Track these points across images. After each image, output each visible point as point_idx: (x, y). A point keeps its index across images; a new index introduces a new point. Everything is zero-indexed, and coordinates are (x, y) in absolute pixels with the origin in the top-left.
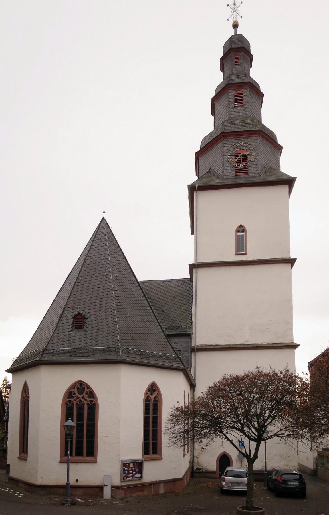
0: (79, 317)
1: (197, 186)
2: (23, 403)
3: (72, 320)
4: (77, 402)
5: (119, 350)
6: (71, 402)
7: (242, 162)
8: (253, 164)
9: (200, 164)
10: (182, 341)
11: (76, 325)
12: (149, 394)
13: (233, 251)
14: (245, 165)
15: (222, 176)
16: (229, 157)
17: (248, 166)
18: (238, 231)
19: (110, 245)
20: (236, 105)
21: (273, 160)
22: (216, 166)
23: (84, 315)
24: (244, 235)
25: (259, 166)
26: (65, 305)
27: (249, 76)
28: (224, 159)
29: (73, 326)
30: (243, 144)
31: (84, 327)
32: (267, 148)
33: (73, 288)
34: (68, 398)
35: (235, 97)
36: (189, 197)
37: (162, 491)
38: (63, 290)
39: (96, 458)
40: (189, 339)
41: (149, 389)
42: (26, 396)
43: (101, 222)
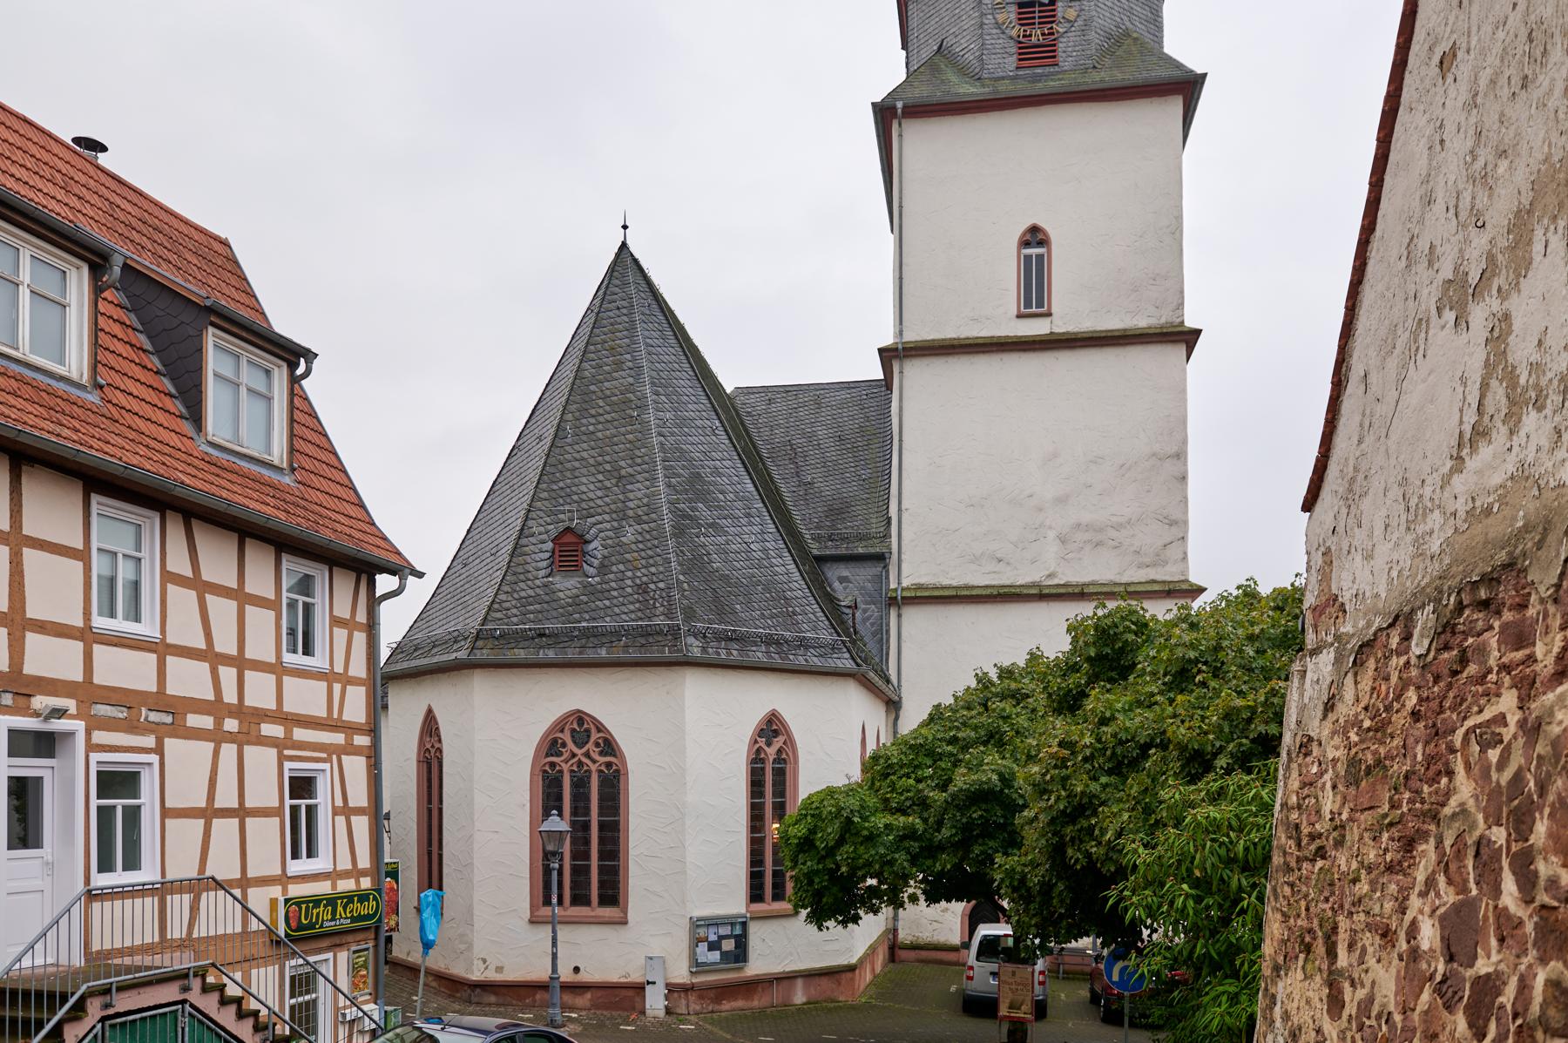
0: (569, 538)
1: (899, 105)
2: (425, 765)
3: (550, 545)
4: (572, 765)
5: (680, 629)
6: (555, 766)
7: (1039, 23)
8: (1073, 29)
9: (913, 23)
11: (560, 561)
12: (762, 742)
13: (1011, 303)
14: (1049, 34)
15: (977, 70)
17: (1056, 36)
18: (1025, 243)
19: (645, 326)
22: (960, 37)
23: (580, 533)
25: (1092, 35)
26: (528, 502)
28: (983, 15)
31: (582, 566)
33: (548, 456)
36: (878, 136)
37: (799, 997)
39: (625, 912)
41: (762, 730)
42: (433, 746)
43: (618, 255)
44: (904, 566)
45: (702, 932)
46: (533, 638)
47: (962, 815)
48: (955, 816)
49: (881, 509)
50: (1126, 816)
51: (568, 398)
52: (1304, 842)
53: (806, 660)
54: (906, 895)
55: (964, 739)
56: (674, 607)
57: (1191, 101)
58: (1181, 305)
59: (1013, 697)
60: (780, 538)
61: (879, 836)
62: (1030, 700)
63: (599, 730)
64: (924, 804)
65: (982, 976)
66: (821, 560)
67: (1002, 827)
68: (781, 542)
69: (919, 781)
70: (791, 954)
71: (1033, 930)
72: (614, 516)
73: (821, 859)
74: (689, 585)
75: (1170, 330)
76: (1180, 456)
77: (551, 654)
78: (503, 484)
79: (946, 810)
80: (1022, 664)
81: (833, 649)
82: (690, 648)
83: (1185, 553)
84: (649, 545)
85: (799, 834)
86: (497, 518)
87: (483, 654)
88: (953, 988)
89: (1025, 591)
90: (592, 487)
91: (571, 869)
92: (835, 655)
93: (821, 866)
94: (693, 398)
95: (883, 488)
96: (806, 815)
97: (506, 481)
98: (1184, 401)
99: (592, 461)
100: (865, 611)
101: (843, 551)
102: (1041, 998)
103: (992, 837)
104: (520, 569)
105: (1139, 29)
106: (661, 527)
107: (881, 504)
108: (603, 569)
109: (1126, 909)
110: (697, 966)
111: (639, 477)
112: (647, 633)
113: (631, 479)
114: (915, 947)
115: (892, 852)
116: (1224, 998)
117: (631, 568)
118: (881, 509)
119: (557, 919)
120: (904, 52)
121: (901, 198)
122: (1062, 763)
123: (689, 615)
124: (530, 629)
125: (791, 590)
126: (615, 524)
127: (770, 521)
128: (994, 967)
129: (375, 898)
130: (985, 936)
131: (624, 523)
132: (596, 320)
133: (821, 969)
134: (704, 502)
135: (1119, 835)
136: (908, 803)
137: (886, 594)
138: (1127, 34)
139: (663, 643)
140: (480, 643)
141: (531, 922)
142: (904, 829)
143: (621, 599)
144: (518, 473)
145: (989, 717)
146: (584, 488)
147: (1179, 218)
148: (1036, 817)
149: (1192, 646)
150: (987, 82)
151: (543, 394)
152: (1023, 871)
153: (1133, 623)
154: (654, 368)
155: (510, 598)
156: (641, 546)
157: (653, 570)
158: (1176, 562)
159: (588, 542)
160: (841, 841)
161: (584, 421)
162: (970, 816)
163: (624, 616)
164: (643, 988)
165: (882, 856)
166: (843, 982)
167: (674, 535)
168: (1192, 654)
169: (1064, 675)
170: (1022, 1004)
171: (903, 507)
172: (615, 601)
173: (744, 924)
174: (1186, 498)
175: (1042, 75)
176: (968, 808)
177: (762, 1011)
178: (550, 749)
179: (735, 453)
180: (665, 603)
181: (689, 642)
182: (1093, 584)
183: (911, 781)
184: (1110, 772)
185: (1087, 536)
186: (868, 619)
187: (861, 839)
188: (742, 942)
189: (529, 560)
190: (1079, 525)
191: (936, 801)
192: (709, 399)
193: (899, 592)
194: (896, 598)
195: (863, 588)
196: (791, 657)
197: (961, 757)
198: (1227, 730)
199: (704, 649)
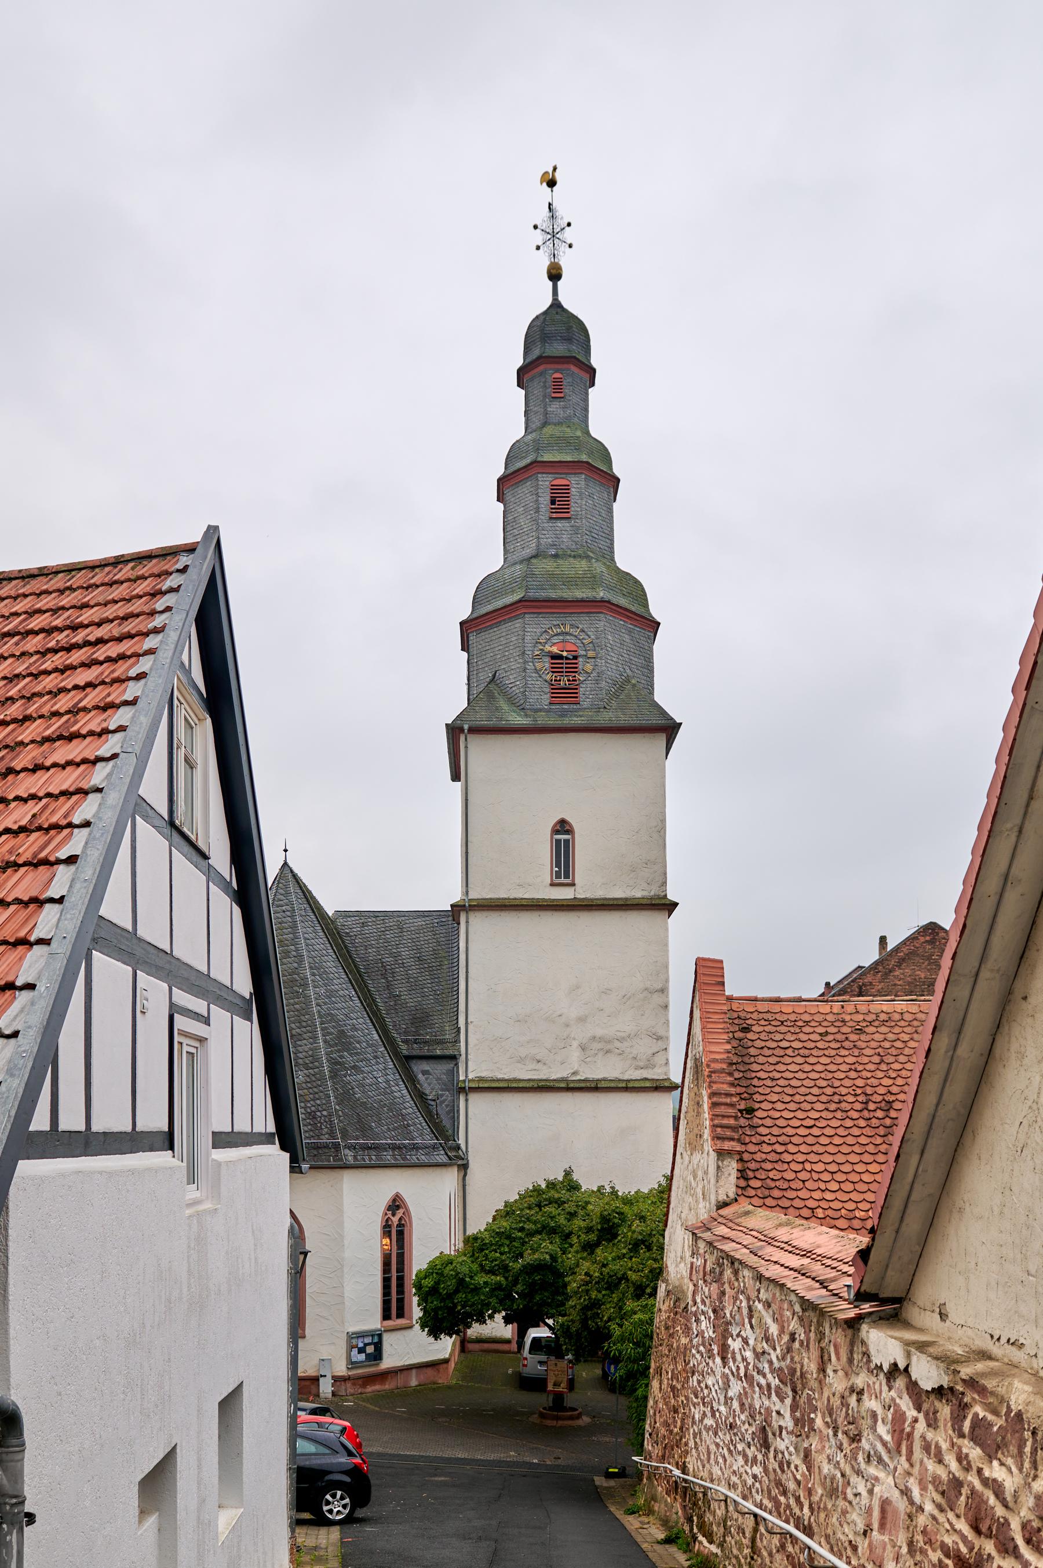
1: (466, 727)
10: (440, 1069)
15: (522, 702)
18: (555, 831)
20: (554, 515)
21: (636, 660)
28: (525, 662)
30: (567, 630)
37: (414, 1382)
44: (470, 1063)
45: (354, 1342)
47: (529, 1278)
49: (452, 1019)
50: (612, 1310)
53: (417, 1158)
55: (529, 1230)
58: (664, 883)
59: (556, 1202)
64: (506, 1268)
65: (532, 1364)
66: (409, 1058)
70: (408, 1353)
73: (443, 1300)
75: (657, 902)
76: (663, 990)
80: (561, 1179)
81: (433, 1148)
83: (667, 1060)
84: (315, 1084)
88: (510, 1371)
89: (557, 1085)
96: (432, 1273)
106: (322, 1072)
107: (452, 1014)
110: (352, 1364)
111: (305, 1036)
113: (299, 1037)
114: (480, 1341)
118: (452, 1019)
120: (465, 655)
122: (587, 1283)
125: (405, 1108)
128: (543, 1358)
130: (534, 1338)
133: (427, 1362)
134: (347, 1050)
135: (609, 1320)
136: (496, 1268)
145: (543, 1216)
147: (663, 821)
150: (529, 713)
153: (617, 1213)
156: (309, 1085)
157: (318, 1102)
160: (457, 1291)
164: (318, 1380)
165: (482, 1300)
166: (441, 1370)
167: (331, 1077)
168: (640, 1237)
169: (587, 1232)
171: (469, 1021)
173: (380, 1336)
174: (668, 1021)
177: (392, 1391)
182: (605, 1080)
184: (606, 1289)
185: (599, 1046)
188: (378, 1346)
192: (347, 974)
194: (464, 1088)
195: (440, 1079)
199: (355, 1157)
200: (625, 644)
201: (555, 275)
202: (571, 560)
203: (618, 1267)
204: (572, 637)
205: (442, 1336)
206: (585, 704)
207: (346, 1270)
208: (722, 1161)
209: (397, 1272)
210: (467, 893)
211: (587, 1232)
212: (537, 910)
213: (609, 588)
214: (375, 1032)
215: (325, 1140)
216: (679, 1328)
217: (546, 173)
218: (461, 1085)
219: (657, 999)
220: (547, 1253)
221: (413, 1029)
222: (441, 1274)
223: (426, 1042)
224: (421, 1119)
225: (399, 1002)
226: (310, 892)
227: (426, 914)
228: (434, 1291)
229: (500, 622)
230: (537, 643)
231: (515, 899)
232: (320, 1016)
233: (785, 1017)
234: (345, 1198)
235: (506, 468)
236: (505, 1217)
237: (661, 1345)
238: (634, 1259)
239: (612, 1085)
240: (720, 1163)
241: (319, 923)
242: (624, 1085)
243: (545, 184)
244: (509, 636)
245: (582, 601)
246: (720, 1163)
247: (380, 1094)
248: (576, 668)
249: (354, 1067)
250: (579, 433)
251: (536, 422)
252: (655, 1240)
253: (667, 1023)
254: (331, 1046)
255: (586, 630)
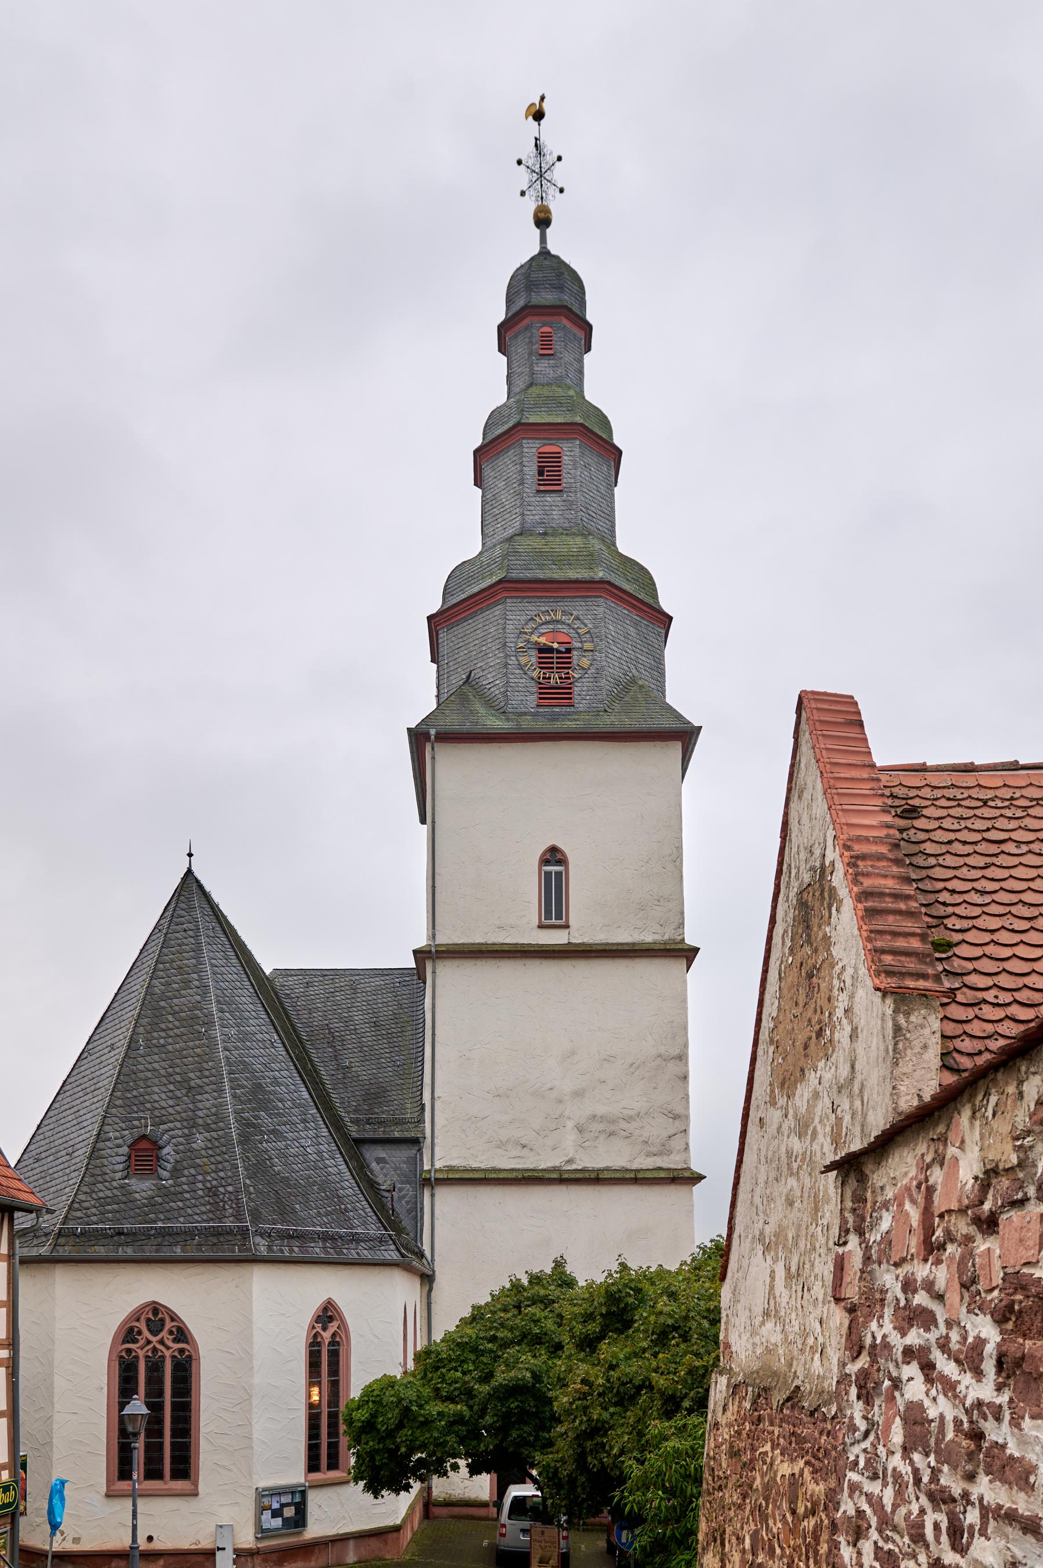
1: (433, 732)
3: (125, 1150)
4: (147, 1351)
5: (248, 1230)
6: (131, 1352)
8: (587, 675)
10: (399, 1156)
11: (136, 1165)
15: (502, 704)
16: (521, 650)
18: (545, 861)
19: (209, 947)
20: (542, 488)
21: (644, 658)
22: (486, 672)
23: (154, 1139)
24: (561, 873)
27: (584, 398)
28: (507, 656)
29: (129, 1166)
31: (156, 1170)
32: (627, 626)
33: (122, 1065)
34: (124, 1342)
35: (539, 462)
37: (351, 1558)
38: (90, 1058)
40: (414, 1152)
41: (318, 1316)
44: (437, 1149)
45: (266, 1501)
46: (112, 1236)
47: (503, 1405)
48: (496, 1405)
49: (415, 1095)
50: (626, 1438)
51: (140, 1013)
52: (716, 1479)
54: (449, 1464)
55: (502, 1339)
56: (242, 1209)
57: (688, 748)
58: (681, 925)
59: (542, 1302)
60: (332, 1141)
61: (433, 1421)
62: (556, 1305)
63: (173, 1320)
64: (469, 1394)
66: (359, 1142)
67: (535, 1415)
68: (333, 1144)
69: (464, 1373)
71: (563, 1510)
72: (185, 1123)
74: (254, 1188)
75: (673, 947)
76: (682, 1057)
77: (130, 1252)
78: (74, 1085)
79: (489, 1400)
80: (548, 1271)
81: (380, 1242)
82: (257, 1247)
83: (687, 1144)
84: (218, 1151)
85: (363, 1418)
86: (70, 1118)
87: (65, 1251)
88: (485, 1543)
89: (547, 1176)
90: (163, 1096)
91: (145, 1446)
92: (383, 1248)
93: (381, 1446)
94: (253, 1013)
95: (416, 1074)
96: (368, 1402)
97: (77, 1083)
98: (685, 1009)
99: (163, 1072)
100: (401, 1190)
101: (380, 1134)
102: (564, 1551)
103: (526, 1423)
104: (98, 1171)
105: (646, 679)
107: (415, 1089)
108: (176, 1172)
109: (626, 1505)
110: (262, 1532)
111: (207, 1088)
112: (218, 1233)
113: (199, 1090)
114: (448, 1504)
115: (445, 1435)
116: (683, 1563)
117: (202, 1172)
118: (415, 1095)
119: (137, 1492)
121: (433, 814)
122: (584, 1396)
123: (256, 1216)
124: (110, 1229)
125: (343, 1188)
126: (186, 1131)
127: (323, 1126)
128: (526, 1524)
129: (14, 1489)
130: (515, 1497)
131: (194, 1130)
132: (164, 940)
134: (265, 1110)
135: (622, 1452)
136: (456, 1393)
137: (421, 1175)
138: (633, 681)
139: (233, 1243)
140: (62, 1240)
141: (108, 1496)
142: (454, 1415)
143: (193, 1201)
144: (90, 1077)
145: (522, 1320)
146: (156, 1097)
147: (679, 848)
148: (566, 1433)
149: (670, 1315)
150: (511, 716)
151: (112, 1003)
152: (556, 1465)
153: (631, 1289)
154: (218, 987)
155: (89, 1199)
156: (210, 1152)
157: (222, 1174)
158: (679, 1152)
159: (161, 1148)
160: (400, 1426)
161: (155, 1034)
162: (509, 1406)
163: (196, 1217)
164: (214, 1554)
167: (240, 1142)
168: (670, 1322)
169: (585, 1322)
170: (550, 1559)
171: (436, 1096)
172: (188, 1203)
173: (303, 1493)
174: (687, 1095)
175: (559, 714)
176: (507, 1399)
178: (126, 1336)
179: (291, 1064)
180: (234, 1206)
181: (256, 1242)
182: (607, 1169)
183: (459, 1374)
184: (616, 1405)
186: (403, 1197)
187: (417, 1424)
188: (301, 1509)
189: (106, 1163)
190: (595, 1116)
191: (481, 1392)
192: (268, 1014)
193: (433, 1175)
194: (430, 1179)
196: (345, 1251)
197: (500, 1353)
198: (689, 1382)
199: (270, 1248)
200: (630, 637)
201: (543, 221)
202: (564, 537)
203: (634, 1369)
204: (564, 626)
205: (383, 1493)
206: (581, 706)
207: (255, 1402)
208: (907, 1014)
209: (329, 1407)
210: (434, 936)
211: (585, 1322)
212: (521, 957)
213: (609, 569)
214: (304, 1089)
215: (229, 1223)
216: (768, 1447)
217: (533, 104)
218: (425, 1175)
219: (673, 1068)
220: (527, 1369)
221: (366, 1107)
222: (378, 1403)
223: (381, 1123)
224: (365, 1203)
225: (350, 1075)
226: (225, 917)
227: (385, 972)
228: (369, 1426)
229: (476, 612)
230: (521, 633)
231: (495, 944)
232: (229, 1063)
233: (990, 794)
234: (254, 1303)
235: (484, 439)
236: (471, 1323)
237: (720, 1488)
238: (661, 1356)
239: (618, 1175)
240: (902, 1020)
241: (233, 947)
242: (632, 1176)
243: (530, 118)
244: (487, 627)
245: (577, 581)
246: (902, 1020)
247: (309, 1168)
248: (570, 663)
249: (274, 1132)
250: (571, 393)
251: (520, 384)
252: (694, 1325)
253: (686, 1097)
254: (242, 1103)
255: (581, 617)
